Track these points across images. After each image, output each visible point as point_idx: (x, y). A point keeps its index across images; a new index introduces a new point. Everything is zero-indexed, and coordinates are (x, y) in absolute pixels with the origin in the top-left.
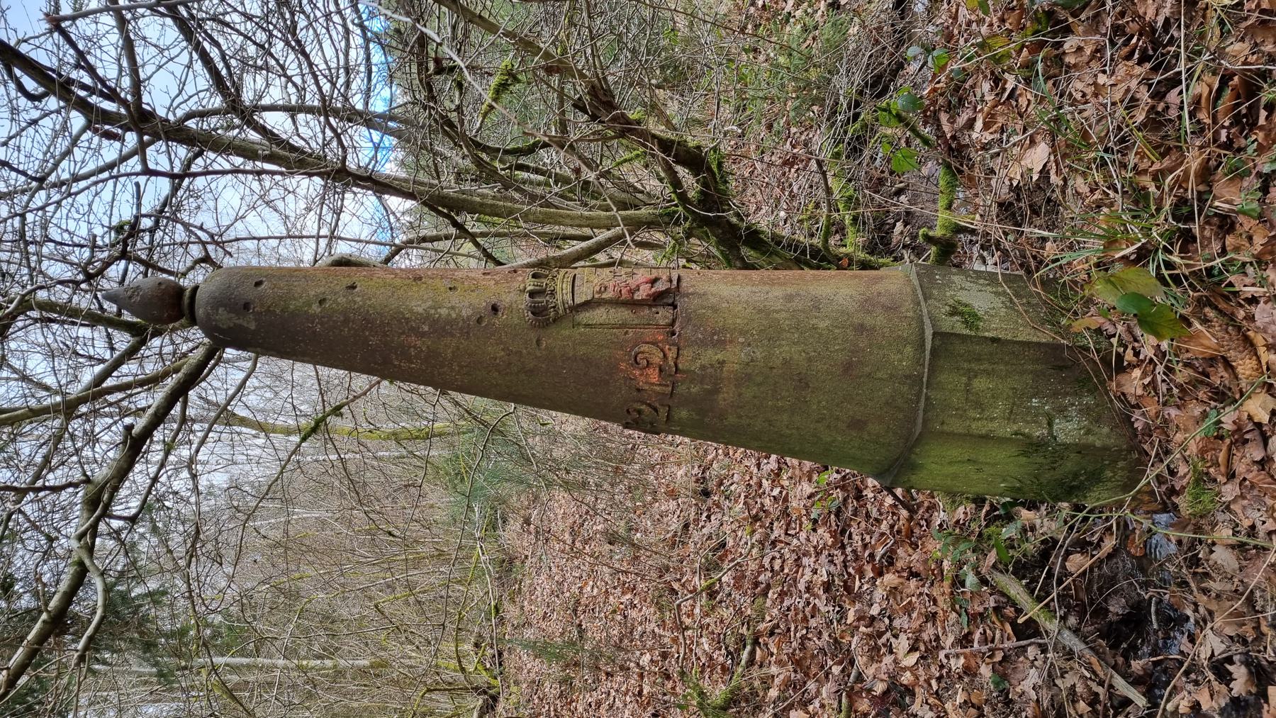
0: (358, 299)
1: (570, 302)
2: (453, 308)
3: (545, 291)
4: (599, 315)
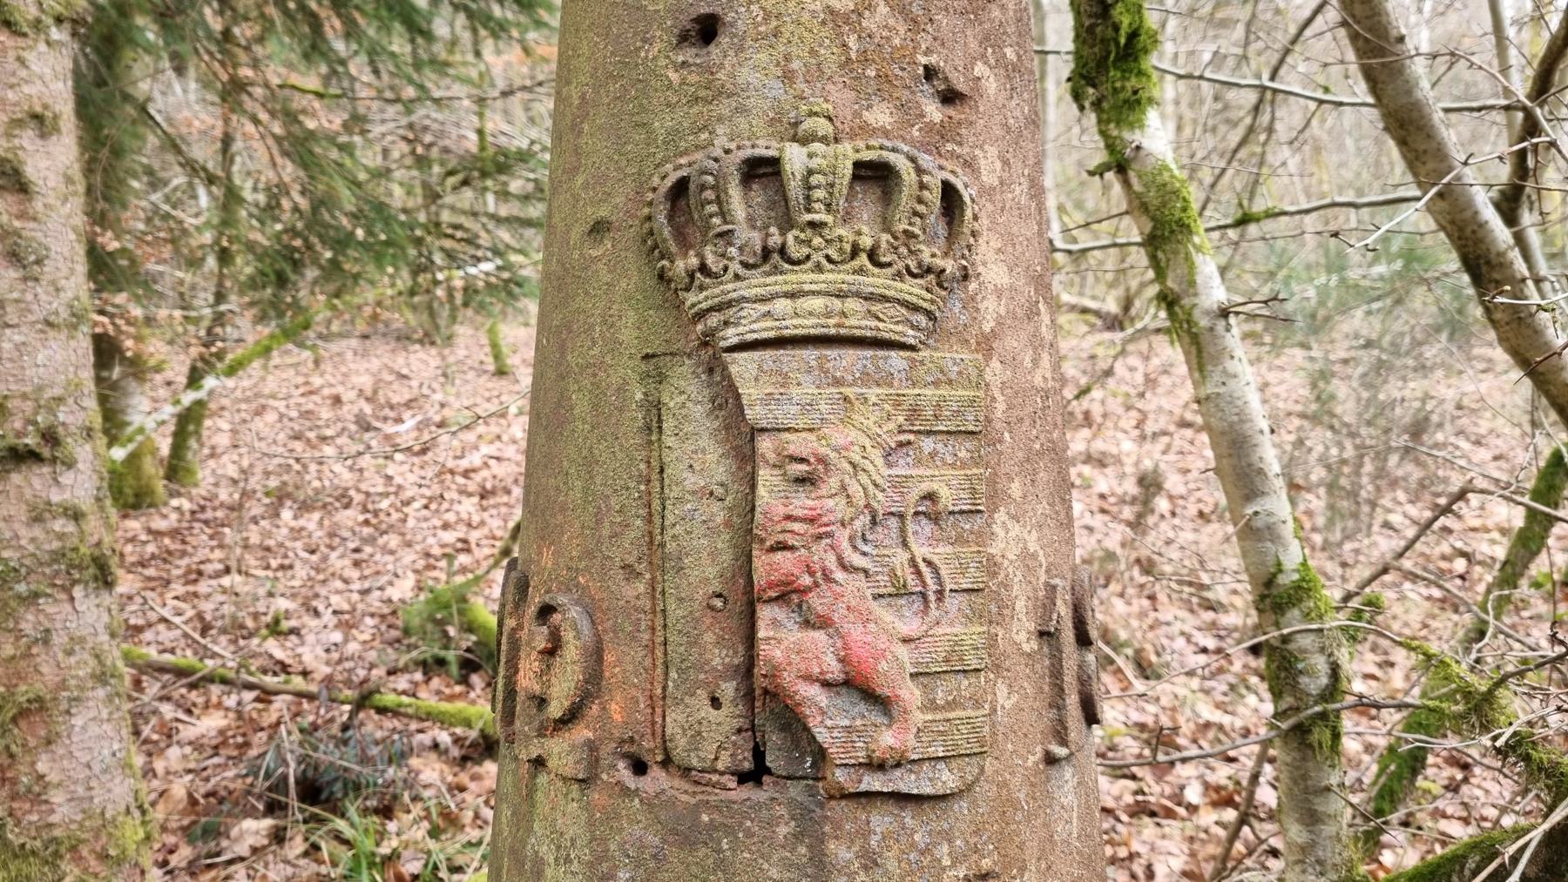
4: (696, 457)
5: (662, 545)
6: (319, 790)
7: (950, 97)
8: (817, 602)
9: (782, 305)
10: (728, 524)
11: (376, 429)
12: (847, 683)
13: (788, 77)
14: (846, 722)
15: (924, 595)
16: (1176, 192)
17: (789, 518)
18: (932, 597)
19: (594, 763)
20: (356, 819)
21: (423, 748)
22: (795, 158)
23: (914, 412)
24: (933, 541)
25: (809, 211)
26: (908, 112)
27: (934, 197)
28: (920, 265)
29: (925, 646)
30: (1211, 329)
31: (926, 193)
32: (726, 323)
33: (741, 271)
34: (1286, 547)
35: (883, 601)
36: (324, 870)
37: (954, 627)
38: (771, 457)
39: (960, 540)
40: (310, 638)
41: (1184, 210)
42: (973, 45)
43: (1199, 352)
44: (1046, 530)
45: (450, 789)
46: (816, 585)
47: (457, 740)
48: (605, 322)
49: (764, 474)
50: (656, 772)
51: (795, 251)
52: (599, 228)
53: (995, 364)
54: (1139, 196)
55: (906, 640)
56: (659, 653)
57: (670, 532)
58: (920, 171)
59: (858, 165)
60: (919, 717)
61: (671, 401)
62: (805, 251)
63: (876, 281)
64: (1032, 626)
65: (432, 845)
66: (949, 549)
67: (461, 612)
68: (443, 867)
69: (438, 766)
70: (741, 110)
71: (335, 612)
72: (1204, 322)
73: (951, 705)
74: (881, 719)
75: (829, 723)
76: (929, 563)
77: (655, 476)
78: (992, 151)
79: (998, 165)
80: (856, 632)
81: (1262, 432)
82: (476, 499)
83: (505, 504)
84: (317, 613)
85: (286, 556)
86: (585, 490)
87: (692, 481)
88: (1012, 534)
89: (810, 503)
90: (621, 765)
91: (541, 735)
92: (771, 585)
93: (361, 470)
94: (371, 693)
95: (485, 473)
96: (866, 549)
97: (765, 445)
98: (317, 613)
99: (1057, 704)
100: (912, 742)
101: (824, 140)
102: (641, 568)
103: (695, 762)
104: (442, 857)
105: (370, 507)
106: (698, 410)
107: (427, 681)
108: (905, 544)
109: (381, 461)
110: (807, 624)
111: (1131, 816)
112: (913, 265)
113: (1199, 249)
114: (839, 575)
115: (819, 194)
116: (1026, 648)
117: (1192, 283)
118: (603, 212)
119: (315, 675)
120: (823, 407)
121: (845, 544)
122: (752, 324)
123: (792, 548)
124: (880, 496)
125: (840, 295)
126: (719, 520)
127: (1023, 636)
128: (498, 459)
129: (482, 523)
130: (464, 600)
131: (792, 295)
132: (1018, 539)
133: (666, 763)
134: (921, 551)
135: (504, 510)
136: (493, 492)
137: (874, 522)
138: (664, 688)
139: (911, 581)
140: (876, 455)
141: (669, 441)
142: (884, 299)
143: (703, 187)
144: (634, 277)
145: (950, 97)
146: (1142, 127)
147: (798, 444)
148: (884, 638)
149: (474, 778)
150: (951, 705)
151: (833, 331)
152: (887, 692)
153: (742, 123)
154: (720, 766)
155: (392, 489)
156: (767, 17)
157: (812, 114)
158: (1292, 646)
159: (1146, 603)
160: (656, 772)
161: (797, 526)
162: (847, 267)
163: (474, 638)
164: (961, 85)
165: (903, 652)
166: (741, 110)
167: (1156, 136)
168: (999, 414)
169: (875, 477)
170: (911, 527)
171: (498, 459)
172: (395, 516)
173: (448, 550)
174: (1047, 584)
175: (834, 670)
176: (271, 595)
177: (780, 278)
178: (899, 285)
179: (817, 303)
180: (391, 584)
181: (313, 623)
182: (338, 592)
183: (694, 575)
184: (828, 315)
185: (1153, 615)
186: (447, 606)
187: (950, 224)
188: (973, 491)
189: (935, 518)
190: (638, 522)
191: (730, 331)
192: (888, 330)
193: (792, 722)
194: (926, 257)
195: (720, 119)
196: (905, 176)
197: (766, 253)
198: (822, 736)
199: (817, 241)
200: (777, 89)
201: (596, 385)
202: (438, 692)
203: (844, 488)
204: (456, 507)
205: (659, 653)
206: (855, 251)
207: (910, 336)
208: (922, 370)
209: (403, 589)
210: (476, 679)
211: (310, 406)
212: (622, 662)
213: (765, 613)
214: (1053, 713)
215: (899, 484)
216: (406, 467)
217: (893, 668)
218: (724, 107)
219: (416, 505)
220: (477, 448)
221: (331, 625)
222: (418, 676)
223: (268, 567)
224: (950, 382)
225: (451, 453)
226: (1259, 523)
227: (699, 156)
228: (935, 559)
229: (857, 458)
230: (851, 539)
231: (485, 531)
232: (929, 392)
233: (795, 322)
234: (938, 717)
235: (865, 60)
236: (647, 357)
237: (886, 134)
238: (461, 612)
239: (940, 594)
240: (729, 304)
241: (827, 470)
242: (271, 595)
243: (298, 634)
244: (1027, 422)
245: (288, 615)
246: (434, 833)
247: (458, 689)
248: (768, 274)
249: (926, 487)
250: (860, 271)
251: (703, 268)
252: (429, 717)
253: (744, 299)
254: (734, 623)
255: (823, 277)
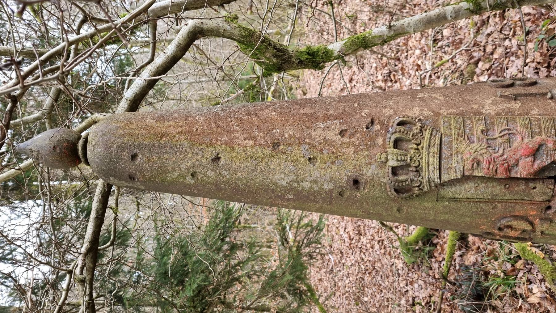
0: (225, 173)
1: (437, 180)
2: (315, 182)
3: (409, 165)
4: (468, 190)
5: (488, 199)
6: (478, 294)
7: (372, 122)
8: (512, 162)
9: (431, 168)
10: (486, 183)
11: (332, 268)
12: (534, 155)
13: (370, 164)
14: (545, 156)
15: (510, 134)
16: (353, 41)
17: (488, 169)
18: (510, 132)
19: (546, 219)
20: (489, 283)
21: (462, 260)
22: (392, 163)
23: (459, 135)
24: (494, 131)
25: (407, 160)
26: (378, 134)
27: (402, 128)
28: (420, 133)
29: (524, 134)
30: (394, 31)
31: (402, 130)
32: (434, 181)
33: (421, 177)
34: (462, 7)
35: (511, 145)
36: (508, 295)
37: (519, 125)
38: (470, 172)
39: (493, 123)
40: (417, 294)
41: (358, 39)
42: (358, 116)
43: (400, 34)
44: (484, 97)
45: (479, 252)
46: (507, 162)
47: (460, 249)
48: (425, 210)
49: (475, 174)
50: (551, 204)
51: (417, 164)
52: (399, 210)
53: (441, 112)
54: (352, 51)
55: (523, 139)
56: (518, 201)
57: (486, 197)
58: (396, 132)
59: (394, 148)
60: (544, 136)
61: (450, 195)
62: (417, 161)
63: (425, 144)
64: (513, 102)
65: (500, 260)
66: (496, 127)
67: (411, 245)
68: (509, 257)
69: (469, 256)
70: (378, 174)
71: (406, 286)
72: (392, 33)
73: (540, 127)
74: (544, 146)
75: (545, 160)
76: (501, 132)
77: (469, 200)
78: (384, 111)
79: (387, 109)
80: (520, 153)
81: (426, 15)
82: (362, 237)
83: (364, 227)
84: (407, 291)
85: (383, 300)
86: (469, 217)
87: (473, 191)
88: (488, 108)
89: (485, 163)
90: (548, 212)
91: (535, 232)
92: (506, 174)
93: (349, 274)
94: (443, 276)
95: (351, 233)
96: (497, 149)
97: (467, 173)
98: (407, 291)
99: (534, 95)
100: (551, 139)
101: (387, 155)
102: (494, 205)
103: (551, 194)
104: (505, 257)
105: (364, 272)
106: (454, 189)
107: (435, 257)
108: (495, 139)
109: (345, 267)
110: (517, 165)
111: (505, 20)
112: (420, 135)
113: (370, 35)
114: (505, 156)
115: (403, 158)
116: (520, 104)
117: (381, 36)
118: (395, 209)
119: (431, 294)
120: (458, 158)
121: (497, 155)
122: (435, 176)
123: (497, 168)
124: (483, 145)
125: (429, 153)
126: (484, 185)
127: (516, 105)
128: (345, 229)
129: (372, 235)
130: (407, 243)
131: (428, 165)
132: (489, 106)
133: (549, 201)
134: (497, 135)
135: (366, 228)
136: (359, 231)
137: (490, 147)
138: (528, 200)
139: (505, 138)
140: (472, 145)
141: (461, 196)
142: (430, 142)
143: (398, 186)
144: (416, 203)
145: (372, 122)
146: (333, 51)
147: (468, 166)
148: (522, 145)
149: (474, 243)
150: (540, 127)
151: (438, 155)
152: (537, 145)
153: (380, 175)
154: (552, 188)
155: (357, 264)
156: (356, 168)
157: (380, 158)
158: (492, 4)
159: (417, 8)
160: (551, 204)
161: (491, 167)
162: (421, 151)
163: (420, 242)
164: (369, 120)
165: (526, 140)
166: (378, 174)
167: (336, 47)
168: (455, 111)
169: (478, 146)
170: (490, 137)
171: (345, 229)
172: (368, 264)
173: (383, 247)
174: (500, 97)
175: (530, 159)
176: (399, 305)
177: (424, 168)
178: (426, 138)
179: (431, 159)
180: (396, 267)
181: (410, 293)
182: (399, 284)
183: (498, 192)
184: (434, 157)
185: (422, 6)
186: (409, 249)
187: (406, 124)
188: (479, 120)
189: (488, 130)
190: (481, 205)
191: (436, 180)
192: (437, 141)
193: (543, 169)
194: (418, 131)
195: (379, 180)
196: (398, 136)
197: (417, 171)
198: (548, 162)
199: (415, 158)
200: (373, 166)
201: (441, 213)
202: (440, 254)
203: (481, 155)
204: (364, 243)
205: (518, 201)
206: (417, 149)
207: (438, 135)
208: (447, 133)
209: (399, 264)
210: (435, 241)
211: (323, 289)
212: (519, 211)
213: (513, 175)
214: (538, 96)
215: (479, 140)
216: (348, 259)
217: (530, 143)
218: (376, 179)
219: (363, 257)
220: (341, 235)
221: (411, 287)
222: (433, 260)
223: (388, 306)
224: (450, 125)
225: (343, 244)
226: (454, 15)
227: (388, 186)
228: (500, 131)
229: (473, 151)
230: (495, 153)
231: (375, 235)
232: (453, 131)
233: (435, 165)
234: (543, 131)
235: (366, 145)
236: (437, 200)
237: (384, 140)
238: (411, 245)
239: (509, 130)
240: (429, 181)
241: (476, 159)
242: (399, 305)
243: (415, 298)
244: (455, 102)
245: (407, 301)
246: (496, 259)
247: (438, 247)
248: (422, 171)
249: (479, 133)
250: (422, 148)
251: (418, 186)
252: (452, 258)
253: (428, 177)
254: (513, 182)
255: (424, 158)
